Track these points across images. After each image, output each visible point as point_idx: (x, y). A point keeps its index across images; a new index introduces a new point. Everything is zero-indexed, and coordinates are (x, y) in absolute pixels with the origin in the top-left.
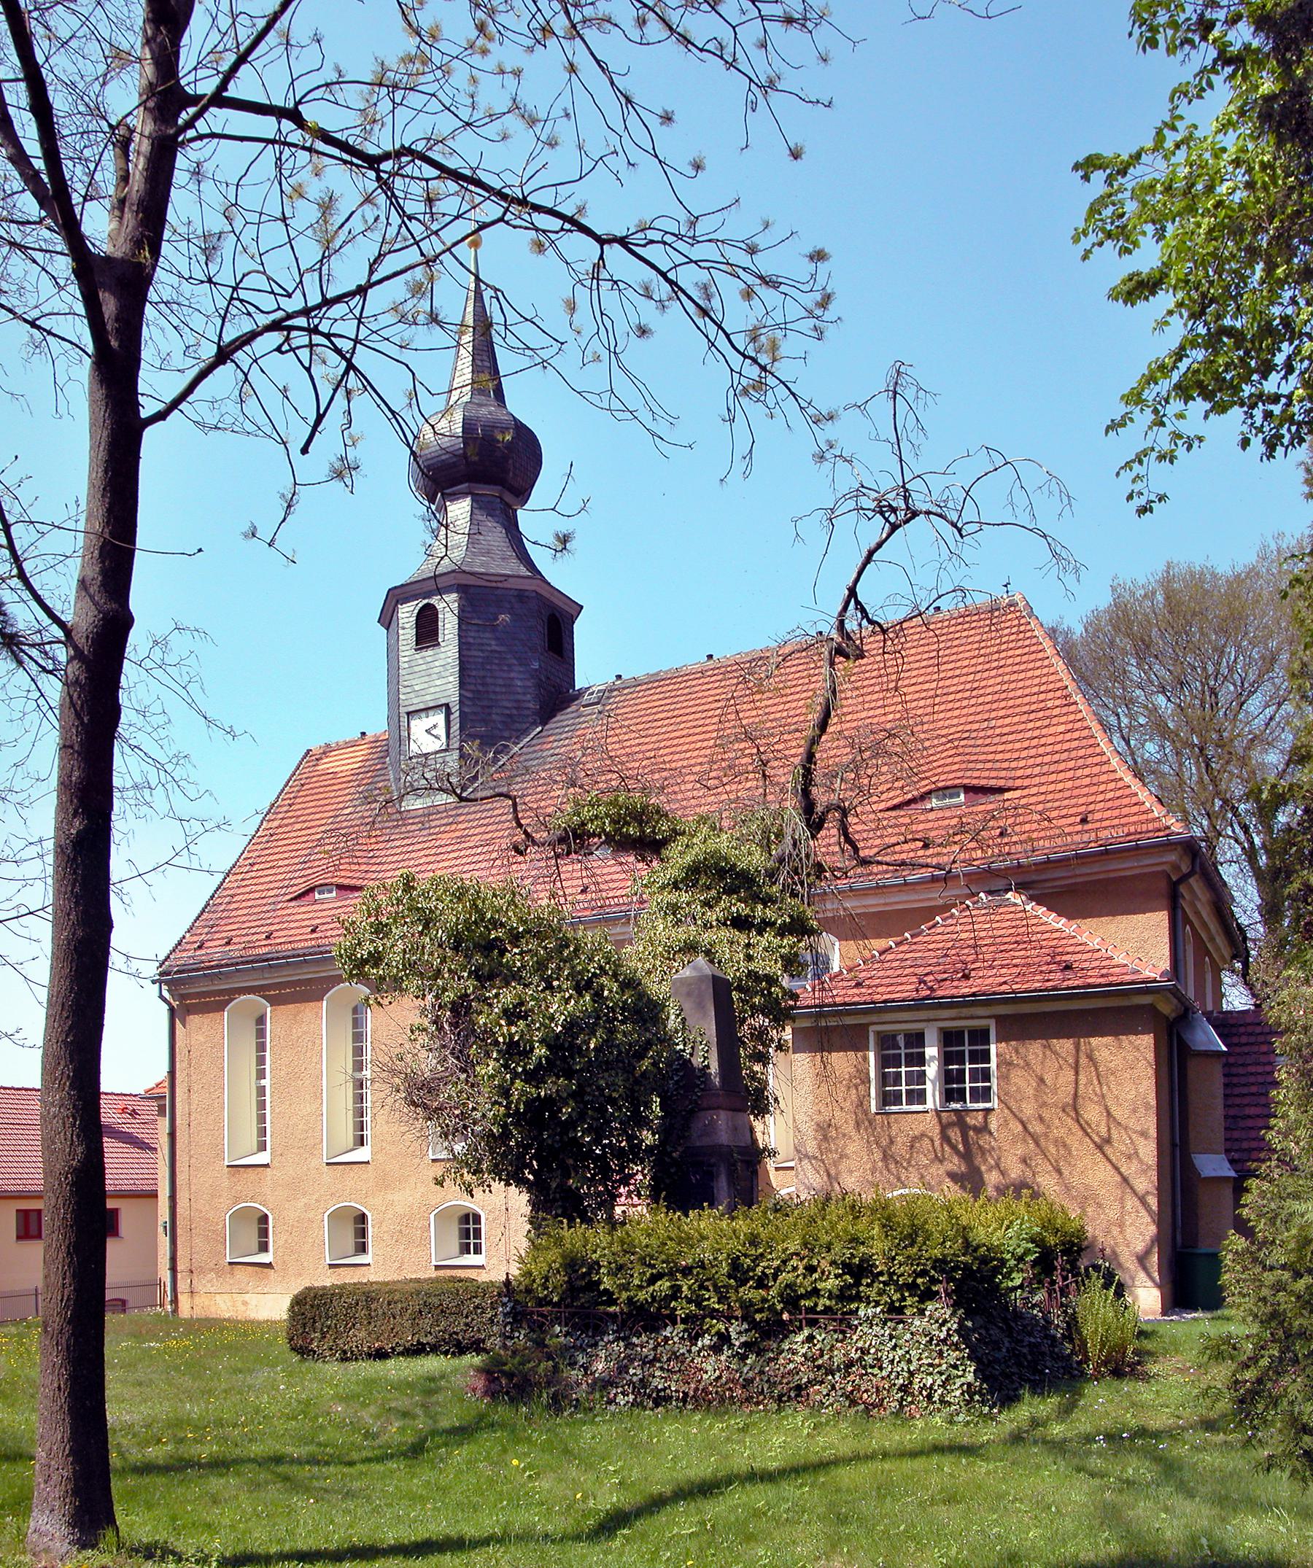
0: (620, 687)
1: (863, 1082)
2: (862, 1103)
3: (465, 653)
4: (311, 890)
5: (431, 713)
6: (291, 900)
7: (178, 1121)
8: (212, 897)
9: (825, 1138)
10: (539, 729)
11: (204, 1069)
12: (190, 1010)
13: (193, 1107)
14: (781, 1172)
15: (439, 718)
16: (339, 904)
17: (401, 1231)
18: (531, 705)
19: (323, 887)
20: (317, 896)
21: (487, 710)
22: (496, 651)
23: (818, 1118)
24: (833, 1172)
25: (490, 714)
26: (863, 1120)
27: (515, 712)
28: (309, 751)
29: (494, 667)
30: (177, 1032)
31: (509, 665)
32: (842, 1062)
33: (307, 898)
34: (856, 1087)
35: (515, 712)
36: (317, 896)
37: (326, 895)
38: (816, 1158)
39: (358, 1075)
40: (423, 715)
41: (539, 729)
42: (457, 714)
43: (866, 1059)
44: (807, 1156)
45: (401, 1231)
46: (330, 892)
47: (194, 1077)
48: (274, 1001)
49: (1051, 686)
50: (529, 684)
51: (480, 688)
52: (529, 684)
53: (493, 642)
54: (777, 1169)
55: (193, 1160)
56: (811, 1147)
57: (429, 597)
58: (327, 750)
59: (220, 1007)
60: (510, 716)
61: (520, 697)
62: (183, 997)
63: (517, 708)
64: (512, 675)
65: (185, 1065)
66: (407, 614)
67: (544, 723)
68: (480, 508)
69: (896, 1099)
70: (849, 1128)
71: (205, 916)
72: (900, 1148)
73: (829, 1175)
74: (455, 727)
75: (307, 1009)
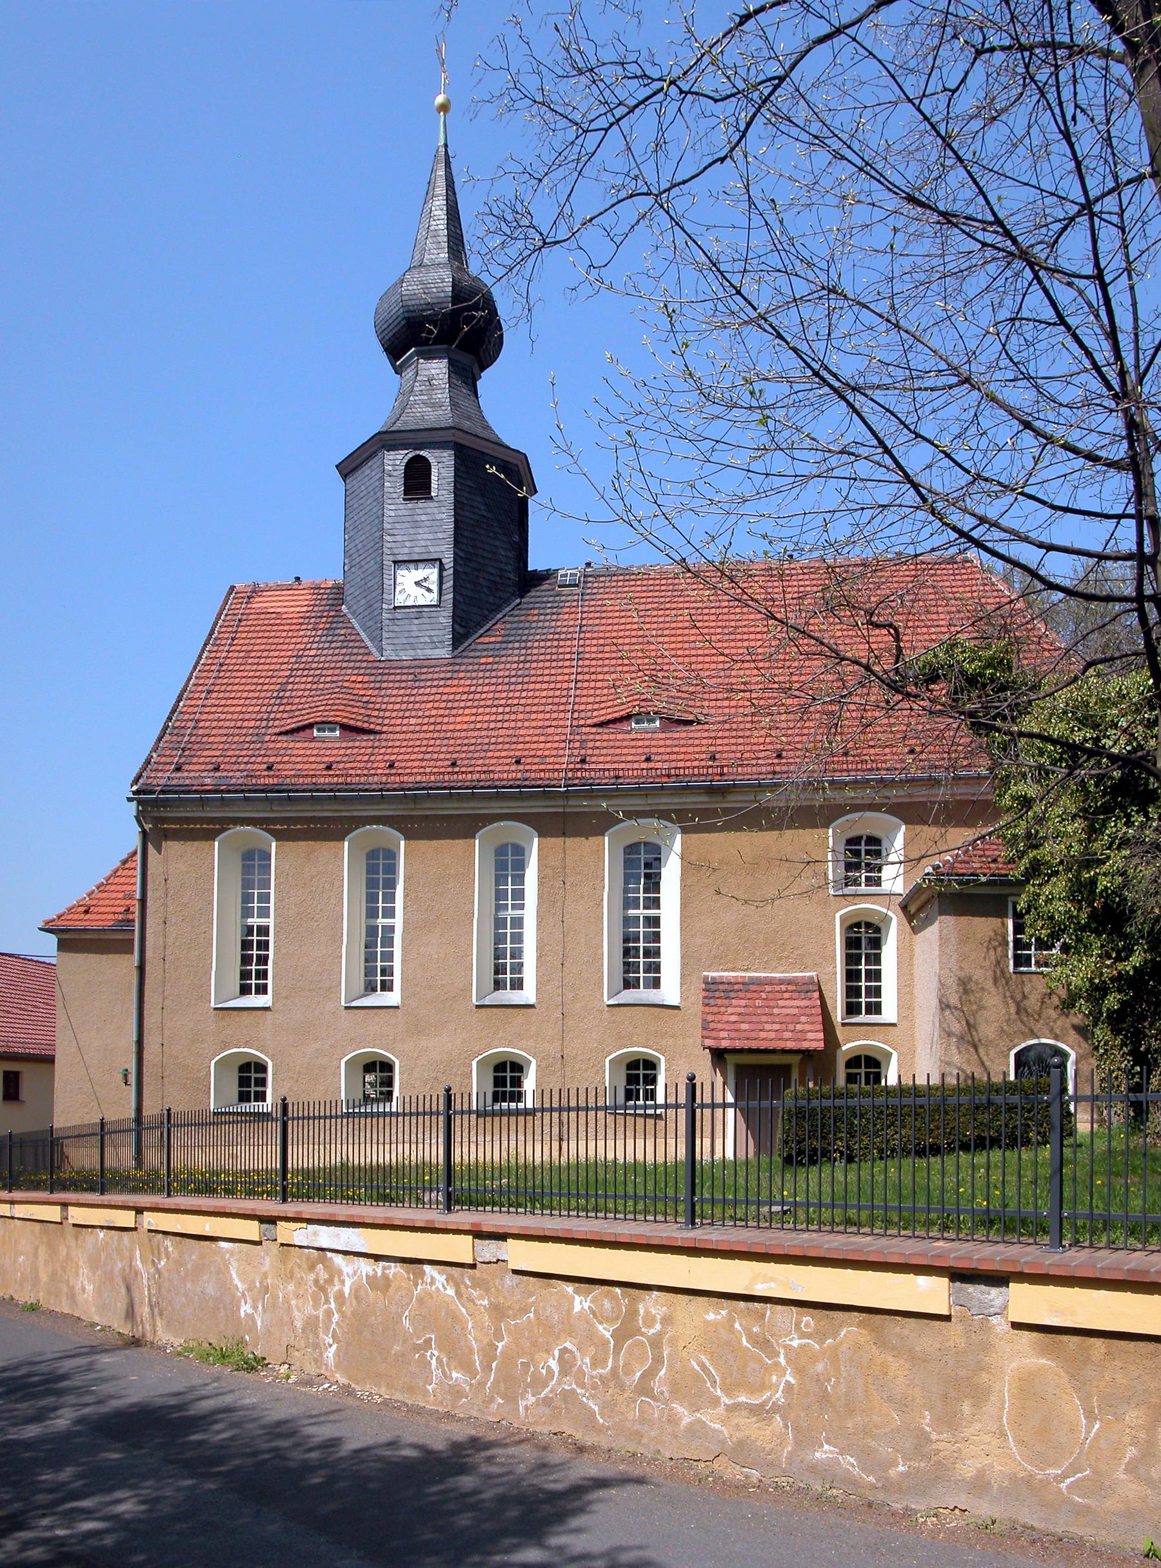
0: (590, 576)
1: (1000, 944)
2: (999, 963)
3: (460, 512)
4: (310, 726)
5: (421, 565)
6: (281, 734)
7: (149, 954)
8: (170, 719)
9: (966, 992)
10: (518, 601)
11: (185, 900)
12: (167, 835)
13: (170, 940)
14: (848, 1028)
15: (433, 573)
16: (344, 745)
17: (436, 1078)
18: (512, 576)
19: (323, 725)
20: (316, 733)
21: (476, 573)
22: (484, 517)
23: (962, 974)
24: (972, 1021)
25: (478, 577)
26: (999, 976)
27: (498, 579)
28: (233, 588)
29: (483, 532)
30: (150, 858)
31: (495, 533)
32: (984, 926)
33: (302, 734)
34: (995, 949)
35: (498, 579)
36: (316, 733)
37: (327, 734)
38: (956, 1008)
39: (372, 922)
40: (412, 566)
41: (518, 601)
42: (451, 571)
43: (1004, 925)
44: (948, 1006)
45: (436, 1078)
46: (333, 730)
47: (171, 908)
48: (279, 836)
49: (397, 685)
50: (510, 555)
51: (471, 550)
52: (510, 555)
53: (482, 507)
54: (843, 1025)
55: (167, 1002)
56: (954, 1000)
57: (421, 449)
58: (255, 591)
59: (210, 836)
60: (495, 583)
61: (503, 566)
62: (157, 821)
63: (501, 576)
64: (498, 543)
65: (161, 893)
66: (396, 461)
67: (522, 597)
68: (456, 373)
69: (1027, 961)
70: (989, 984)
71: (167, 737)
72: (1033, 1002)
73: (967, 1022)
74: (449, 584)
75: (324, 849)
